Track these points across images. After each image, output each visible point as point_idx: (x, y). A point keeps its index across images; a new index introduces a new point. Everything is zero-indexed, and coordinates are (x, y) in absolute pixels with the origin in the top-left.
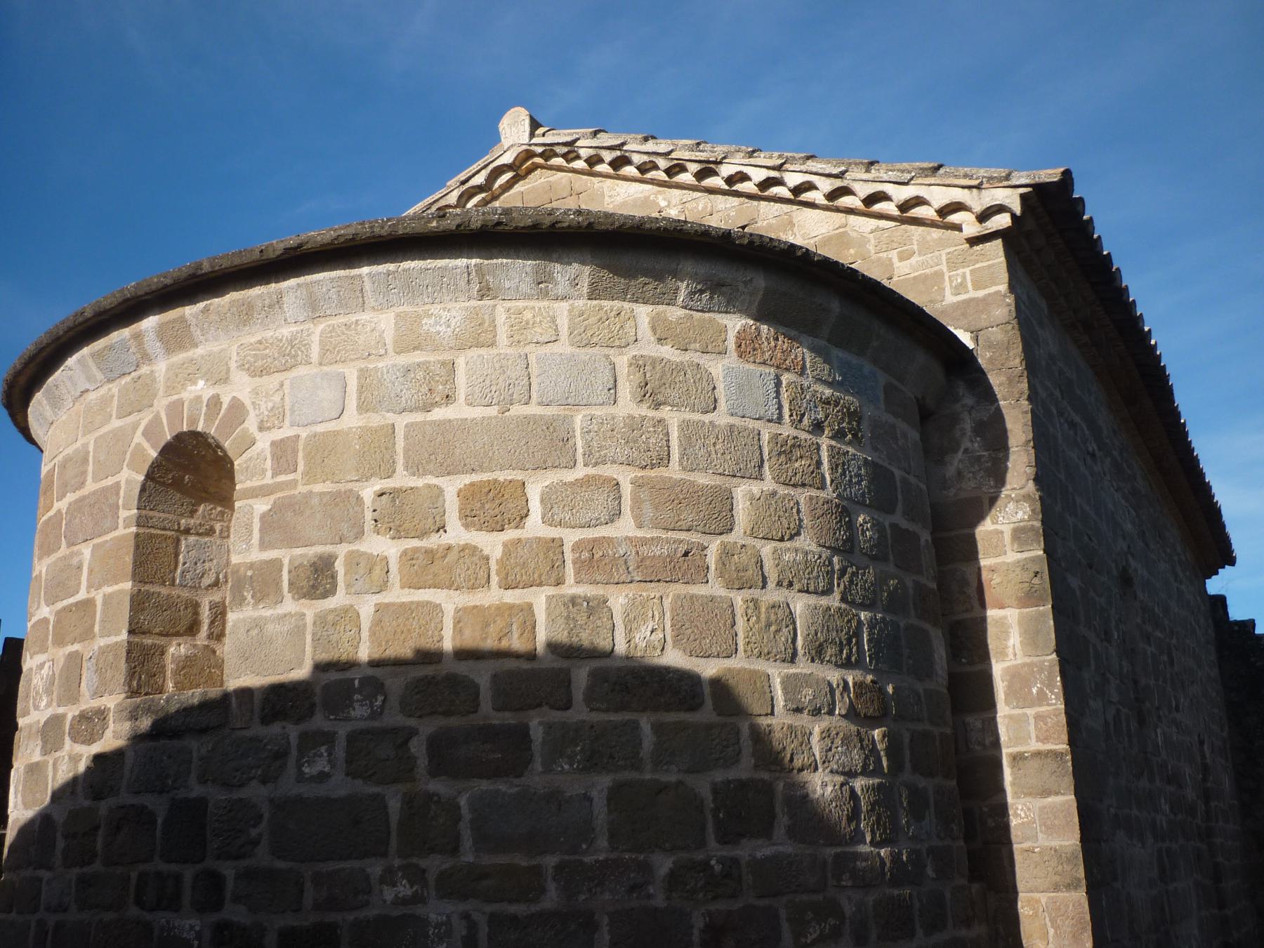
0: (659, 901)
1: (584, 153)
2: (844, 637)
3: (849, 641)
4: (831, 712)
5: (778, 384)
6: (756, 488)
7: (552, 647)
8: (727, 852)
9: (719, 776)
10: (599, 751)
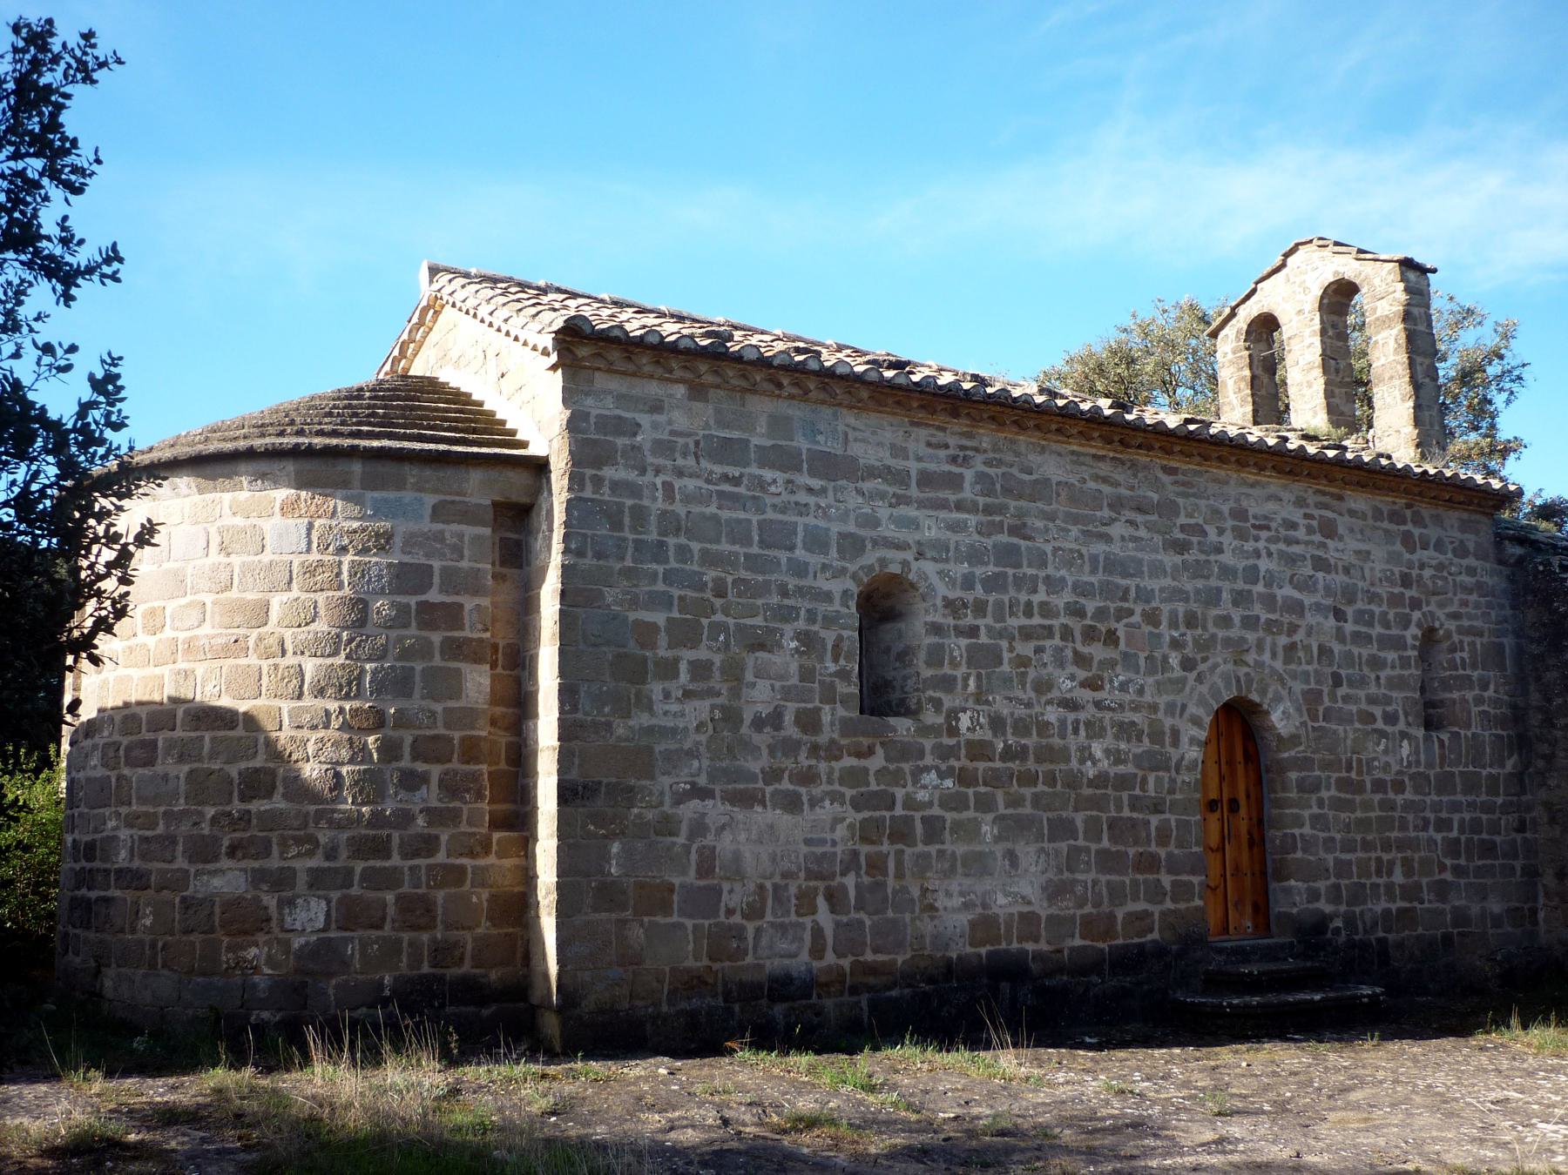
0: (206, 832)
2: (343, 681)
3: (349, 683)
4: (326, 727)
5: (310, 527)
6: (285, 597)
7: (170, 698)
8: (243, 806)
9: (243, 765)
10: (185, 753)
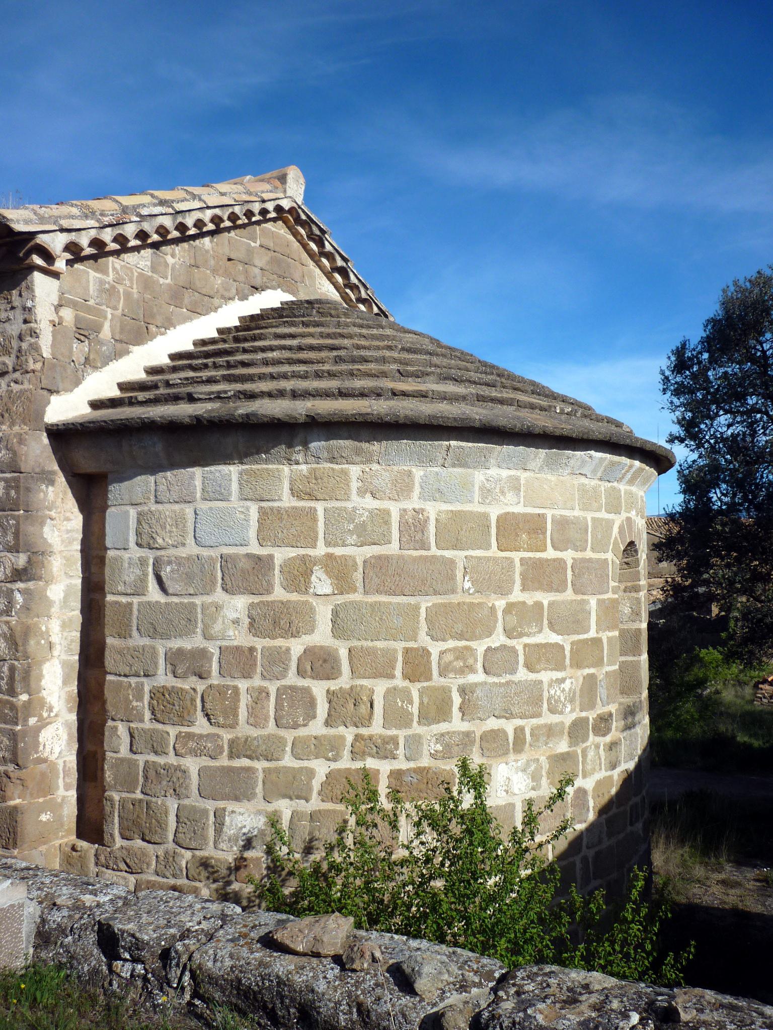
1: (256, 211)
